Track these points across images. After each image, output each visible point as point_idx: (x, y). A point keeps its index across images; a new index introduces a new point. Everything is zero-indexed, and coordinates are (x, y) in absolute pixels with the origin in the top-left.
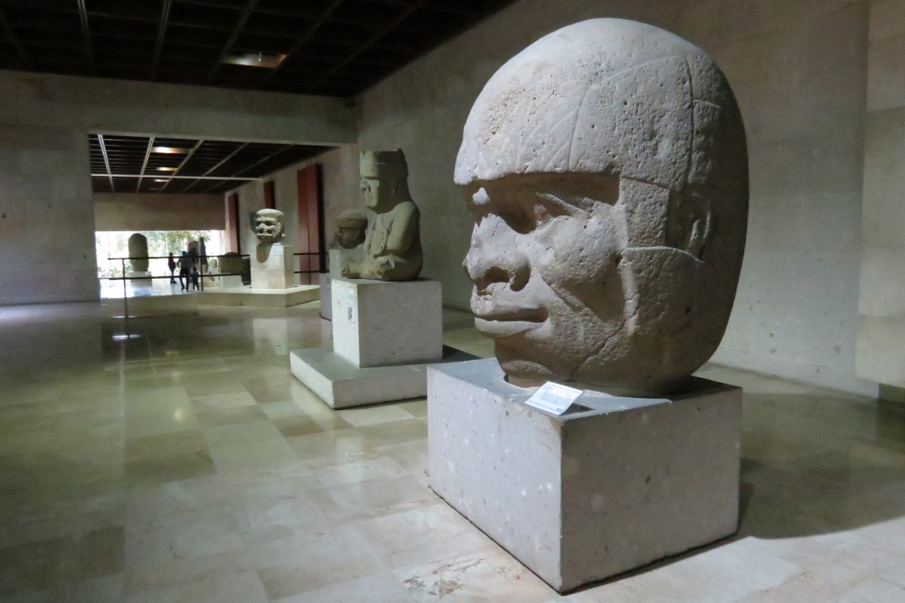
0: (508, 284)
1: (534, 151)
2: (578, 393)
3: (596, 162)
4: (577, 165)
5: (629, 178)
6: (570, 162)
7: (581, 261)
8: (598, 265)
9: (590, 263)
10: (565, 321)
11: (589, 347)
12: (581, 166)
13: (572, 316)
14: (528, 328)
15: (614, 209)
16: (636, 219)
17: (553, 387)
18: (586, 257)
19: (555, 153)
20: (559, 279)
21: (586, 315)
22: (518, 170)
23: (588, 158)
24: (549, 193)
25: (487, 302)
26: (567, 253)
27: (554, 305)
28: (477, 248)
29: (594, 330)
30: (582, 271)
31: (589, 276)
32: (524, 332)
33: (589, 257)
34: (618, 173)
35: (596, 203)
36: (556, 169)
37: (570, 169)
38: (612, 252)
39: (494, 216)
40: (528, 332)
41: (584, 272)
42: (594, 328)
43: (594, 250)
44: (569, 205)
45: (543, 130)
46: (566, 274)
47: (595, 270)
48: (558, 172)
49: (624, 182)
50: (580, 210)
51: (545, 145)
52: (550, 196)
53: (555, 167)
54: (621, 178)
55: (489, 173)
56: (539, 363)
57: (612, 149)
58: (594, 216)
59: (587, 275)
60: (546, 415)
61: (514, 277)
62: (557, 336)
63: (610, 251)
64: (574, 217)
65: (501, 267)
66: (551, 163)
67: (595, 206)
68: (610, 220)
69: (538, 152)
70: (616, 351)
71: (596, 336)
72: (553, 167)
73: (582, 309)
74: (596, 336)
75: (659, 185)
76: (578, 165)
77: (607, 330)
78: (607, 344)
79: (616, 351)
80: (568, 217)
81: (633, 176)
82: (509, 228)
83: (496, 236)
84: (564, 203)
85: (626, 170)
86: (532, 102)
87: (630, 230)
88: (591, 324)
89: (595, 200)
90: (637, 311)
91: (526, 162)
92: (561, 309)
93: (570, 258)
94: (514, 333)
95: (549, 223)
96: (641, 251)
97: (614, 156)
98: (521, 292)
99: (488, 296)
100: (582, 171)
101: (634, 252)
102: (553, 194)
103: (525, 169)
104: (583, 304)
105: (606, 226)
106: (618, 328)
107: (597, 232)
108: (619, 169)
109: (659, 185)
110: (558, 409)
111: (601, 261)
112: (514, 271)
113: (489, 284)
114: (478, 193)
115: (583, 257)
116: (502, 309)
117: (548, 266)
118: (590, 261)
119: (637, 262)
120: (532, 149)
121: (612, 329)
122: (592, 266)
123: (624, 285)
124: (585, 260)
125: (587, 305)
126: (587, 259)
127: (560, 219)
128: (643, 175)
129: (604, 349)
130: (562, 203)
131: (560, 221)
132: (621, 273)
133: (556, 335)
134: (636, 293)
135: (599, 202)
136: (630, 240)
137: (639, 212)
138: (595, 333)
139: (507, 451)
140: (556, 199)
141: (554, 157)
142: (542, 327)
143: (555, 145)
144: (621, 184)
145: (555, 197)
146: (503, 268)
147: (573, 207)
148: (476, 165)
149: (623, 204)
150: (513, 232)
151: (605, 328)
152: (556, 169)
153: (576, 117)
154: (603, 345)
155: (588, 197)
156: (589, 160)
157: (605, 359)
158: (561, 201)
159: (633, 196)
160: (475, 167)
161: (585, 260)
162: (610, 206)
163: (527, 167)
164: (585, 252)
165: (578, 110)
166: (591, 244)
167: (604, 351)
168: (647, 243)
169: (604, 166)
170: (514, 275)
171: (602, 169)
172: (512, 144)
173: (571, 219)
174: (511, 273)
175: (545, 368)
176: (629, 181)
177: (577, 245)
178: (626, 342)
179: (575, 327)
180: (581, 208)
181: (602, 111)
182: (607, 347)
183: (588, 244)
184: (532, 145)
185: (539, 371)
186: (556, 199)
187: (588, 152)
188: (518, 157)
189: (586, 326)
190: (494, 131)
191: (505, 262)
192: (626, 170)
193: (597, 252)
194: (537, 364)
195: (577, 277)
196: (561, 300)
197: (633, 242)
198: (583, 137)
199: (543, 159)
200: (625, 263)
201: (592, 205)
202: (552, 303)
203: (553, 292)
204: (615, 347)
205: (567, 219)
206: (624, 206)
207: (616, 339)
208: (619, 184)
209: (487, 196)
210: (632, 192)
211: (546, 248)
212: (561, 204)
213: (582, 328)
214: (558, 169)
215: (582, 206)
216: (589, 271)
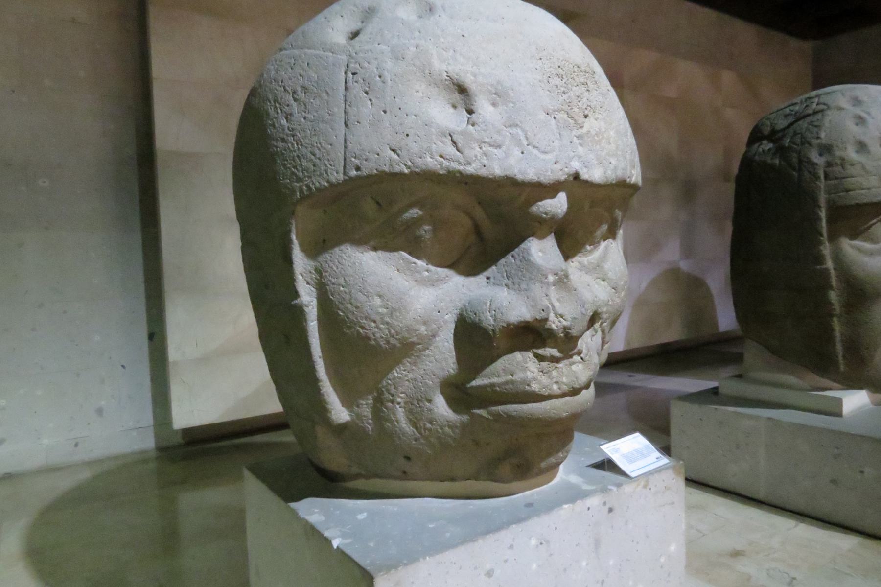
25: (574, 367)
60: (667, 468)
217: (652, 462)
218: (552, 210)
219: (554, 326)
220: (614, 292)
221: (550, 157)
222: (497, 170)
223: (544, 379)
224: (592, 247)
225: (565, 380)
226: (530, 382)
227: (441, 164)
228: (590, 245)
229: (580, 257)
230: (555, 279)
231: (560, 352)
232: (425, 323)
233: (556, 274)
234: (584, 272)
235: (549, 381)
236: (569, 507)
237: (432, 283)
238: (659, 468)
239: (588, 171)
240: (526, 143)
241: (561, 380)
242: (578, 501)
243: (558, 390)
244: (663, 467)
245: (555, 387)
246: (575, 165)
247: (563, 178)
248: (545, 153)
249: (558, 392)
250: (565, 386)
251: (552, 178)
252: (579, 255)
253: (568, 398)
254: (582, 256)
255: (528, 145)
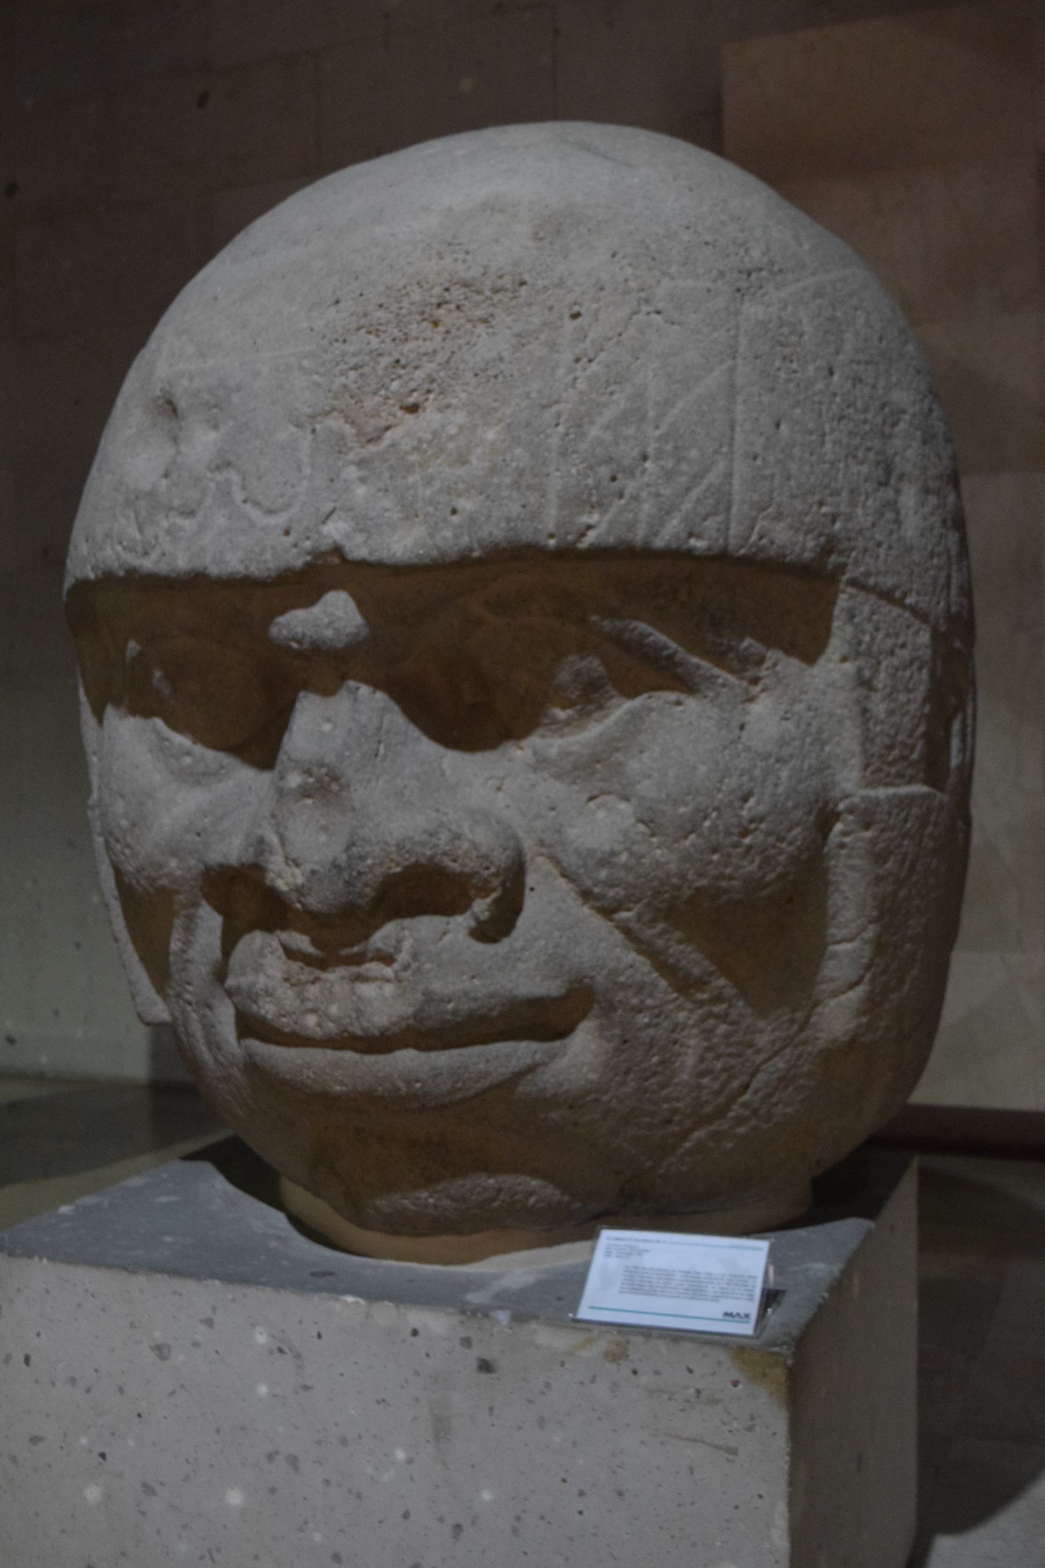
0: (462, 922)
1: (614, 479)
2: (759, 1249)
3: (797, 530)
4: (749, 537)
5: (864, 588)
6: (733, 525)
7: (744, 834)
8: (790, 843)
9: (771, 840)
10: (648, 1026)
11: (704, 1098)
12: (761, 538)
13: (671, 1006)
14: (528, 1061)
15: (814, 677)
16: (879, 707)
17: (642, 1246)
18: (762, 819)
19: (688, 489)
20: (656, 893)
21: (718, 999)
22: (551, 536)
23: (778, 517)
24: (636, 619)
25: (366, 990)
26: (697, 810)
27: (622, 979)
28: (309, 801)
29: (729, 1045)
30: (746, 863)
31: (763, 877)
32: (519, 1076)
33: (769, 818)
34: (842, 568)
35: (773, 655)
36: (693, 542)
37: (731, 548)
38: (820, 805)
39: (364, 690)
40: (529, 1077)
41: (749, 868)
42: (732, 1040)
43: (782, 798)
44: (695, 660)
45: (634, 415)
46: (691, 876)
47: (782, 858)
48: (697, 553)
49: (852, 596)
50: (724, 676)
51: (648, 465)
52: (643, 626)
53: (690, 535)
54: (842, 586)
55: (409, 541)
56: (535, 1173)
57: (829, 500)
58: (763, 695)
59: (759, 874)
60: (726, 1345)
61: (494, 895)
62: (618, 1079)
63: (817, 801)
64: (705, 697)
65: (447, 862)
66: (675, 522)
67: (768, 663)
68: (809, 709)
69: (631, 487)
70: (774, 1100)
71: (733, 1062)
72: (684, 535)
73: (706, 983)
74: (733, 1062)
75: (914, 610)
76: (754, 537)
77: (762, 1040)
78: (755, 1084)
79: (774, 1100)
80: (683, 697)
81: (871, 581)
82: (414, 732)
83: (385, 756)
84: (682, 654)
85: (856, 562)
86: (570, 325)
87: (867, 739)
88: (723, 1028)
89: (769, 646)
90: (868, 976)
91: (582, 513)
92: (640, 988)
93: (707, 823)
94: (485, 1083)
95: (607, 716)
96: (889, 799)
97: (834, 519)
98: (506, 942)
99: (374, 968)
100: (761, 556)
101: (878, 802)
102: (650, 623)
103: (583, 535)
104: (713, 968)
105: (803, 726)
106: (795, 1028)
107: (782, 742)
108: (843, 560)
109: (914, 610)
110: (726, 1314)
111: (798, 830)
112: (496, 875)
113: (378, 927)
114: (316, 610)
115: (752, 821)
116: (450, 1006)
117: (613, 853)
118: (768, 834)
119: (883, 831)
120: (604, 471)
121: (777, 1034)
122: (774, 847)
123: (835, 899)
124: (756, 829)
125: (726, 971)
126: (763, 826)
127: (653, 703)
128: (889, 582)
129: (746, 1097)
130: (676, 652)
131: (651, 710)
132: (832, 863)
133: (617, 1075)
134: (870, 922)
135: (780, 654)
136: (866, 766)
137: (885, 687)
138: (730, 1055)
139: (487, 1496)
140: (659, 637)
141: (687, 506)
142: (565, 1054)
143: (684, 467)
144: (843, 601)
145: (656, 632)
146: (455, 867)
147: (705, 664)
148: (332, 512)
149: (844, 659)
150: (428, 747)
151: (757, 1036)
152: (693, 542)
153: (731, 390)
154: (746, 1087)
155: (753, 636)
156: (782, 525)
157: (742, 1130)
158: (673, 645)
159: (873, 639)
160: (328, 517)
161: (756, 829)
162: (804, 666)
163: (590, 527)
164: (758, 803)
165: (732, 370)
166: (771, 780)
167: (745, 1105)
168: (900, 775)
169: (816, 546)
170: (493, 890)
171: (812, 555)
172: (518, 451)
173: (692, 704)
174: (486, 881)
175: (551, 1187)
176: (862, 596)
177: (730, 783)
178: (806, 1068)
179: (675, 1042)
180: (732, 671)
181: (792, 385)
182: (756, 1092)
183: (764, 780)
184: (609, 460)
185: (532, 1200)
186: (659, 637)
187: (778, 499)
188: (552, 496)
189: (708, 1034)
190: (411, 400)
191: (466, 846)
192: (856, 562)
193: (790, 804)
194: (528, 1179)
195: (724, 884)
196: (641, 958)
197: (874, 773)
198: (758, 449)
199: (647, 508)
200: (845, 834)
201: (761, 661)
202: (616, 972)
203: (619, 936)
204: (776, 1089)
205: (678, 703)
206: (849, 667)
207: (781, 1065)
208: (832, 603)
209: (358, 619)
210: (869, 627)
211: (587, 796)
212: (671, 657)
213: (692, 1042)
214: (698, 544)
215: (735, 663)
216: (766, 861)
217: (709, 1316)
218: (308, 633)
219: (281, 885)
220: (643, 833)
221: (281, 520)
222: (183, 562)
223: (287, 995)
224: (570, 712)
225: (334, 1010)
226: (257, 994)
227: (118, 558)
228: (564, 708)
229: (543, 736)
230: (306, 783)
231: (314, 942)
232: (174, 853)
233: (308, 772)
234: (546, 774)
235: (297, 1003)
236: (357, 1303)
237: (196, 778)
238: (706, 1336)
239: (368, 538)
240: (243, 497)
241: (323, 1008)
242: (386, 1303)
243: (318, 1029)
244: (717, 1338)
245: (311, 1020)
246: (336, 530)
247: (299, 563)
248: (271, 512)
249: (318, 1032)
250: (331, 1025)
251: (271, 565)
252: (540, 731)
253: (349, 1055)
254: (549, 733)
255: (245, 501)
